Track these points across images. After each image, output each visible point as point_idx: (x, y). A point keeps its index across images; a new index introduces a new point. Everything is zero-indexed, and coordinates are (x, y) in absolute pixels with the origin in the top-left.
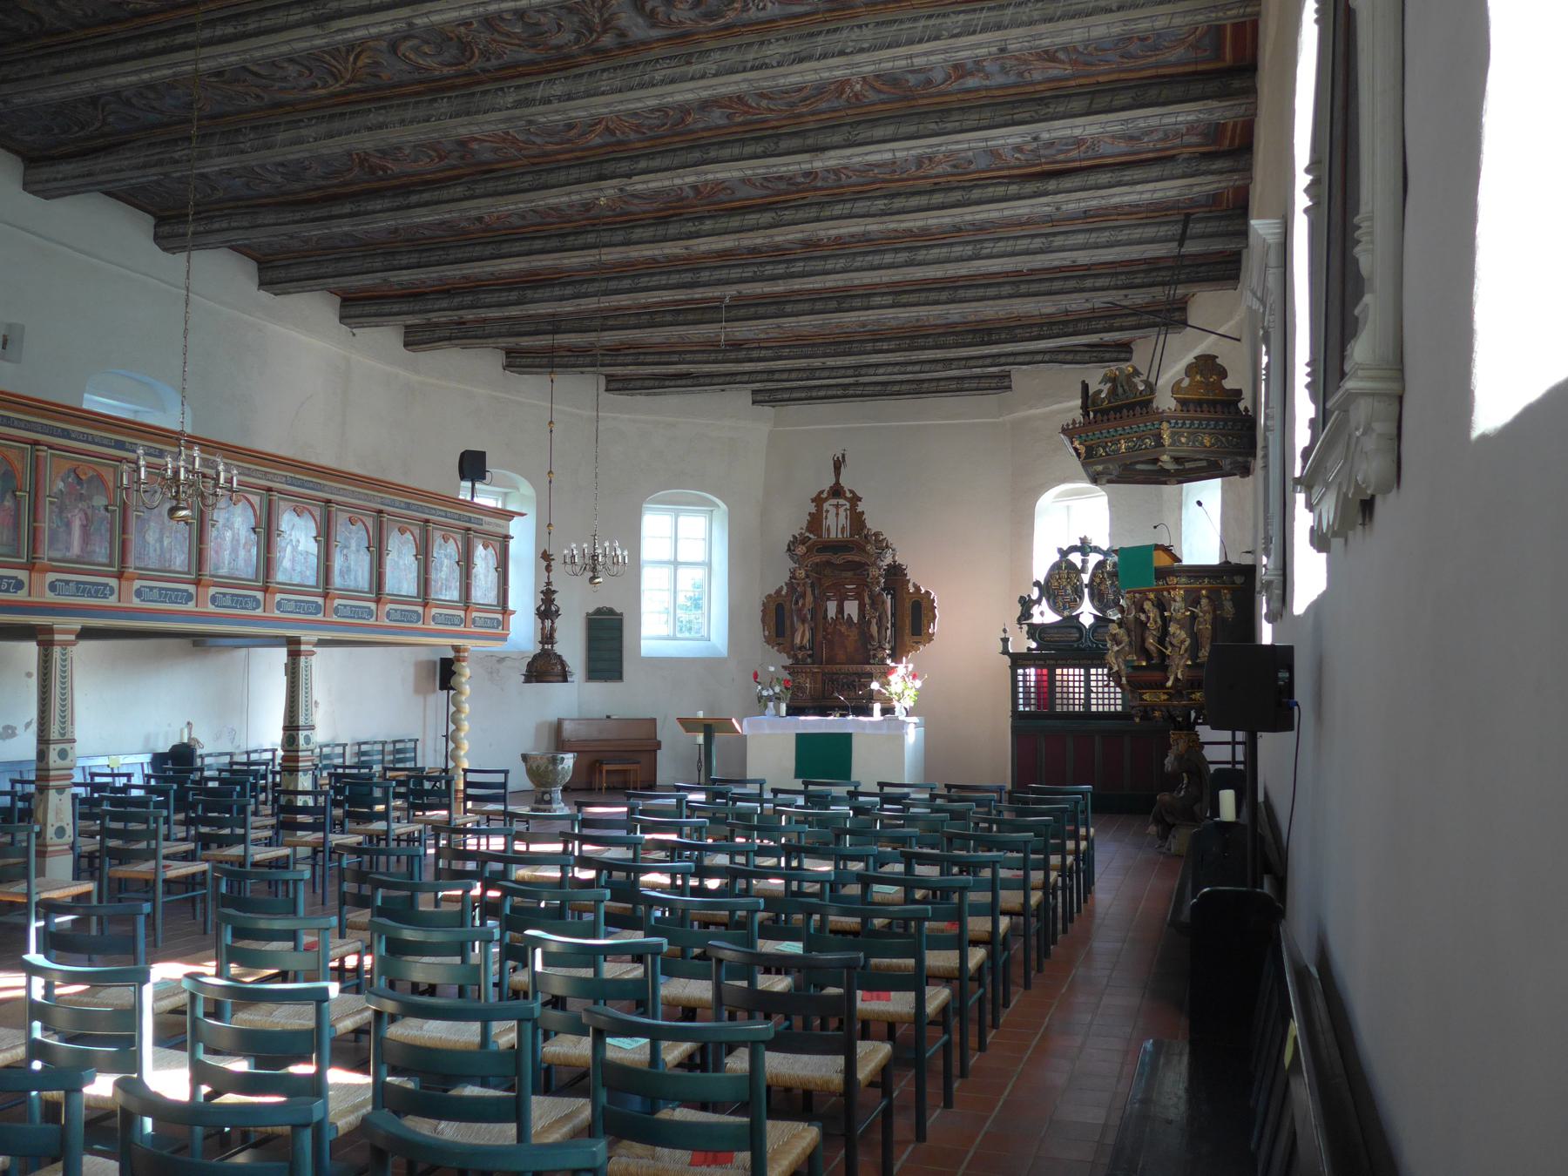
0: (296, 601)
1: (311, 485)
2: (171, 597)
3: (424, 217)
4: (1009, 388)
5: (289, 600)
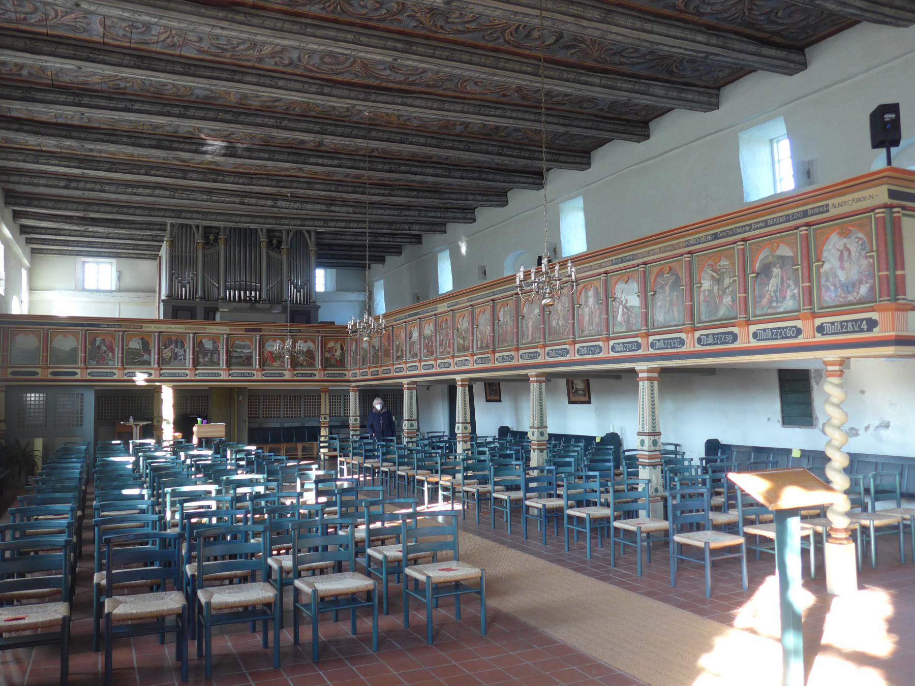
0: (623, 343)
1: (629, 258)
2: (721, 340)
3: (515, 80)
5: (619, 344)
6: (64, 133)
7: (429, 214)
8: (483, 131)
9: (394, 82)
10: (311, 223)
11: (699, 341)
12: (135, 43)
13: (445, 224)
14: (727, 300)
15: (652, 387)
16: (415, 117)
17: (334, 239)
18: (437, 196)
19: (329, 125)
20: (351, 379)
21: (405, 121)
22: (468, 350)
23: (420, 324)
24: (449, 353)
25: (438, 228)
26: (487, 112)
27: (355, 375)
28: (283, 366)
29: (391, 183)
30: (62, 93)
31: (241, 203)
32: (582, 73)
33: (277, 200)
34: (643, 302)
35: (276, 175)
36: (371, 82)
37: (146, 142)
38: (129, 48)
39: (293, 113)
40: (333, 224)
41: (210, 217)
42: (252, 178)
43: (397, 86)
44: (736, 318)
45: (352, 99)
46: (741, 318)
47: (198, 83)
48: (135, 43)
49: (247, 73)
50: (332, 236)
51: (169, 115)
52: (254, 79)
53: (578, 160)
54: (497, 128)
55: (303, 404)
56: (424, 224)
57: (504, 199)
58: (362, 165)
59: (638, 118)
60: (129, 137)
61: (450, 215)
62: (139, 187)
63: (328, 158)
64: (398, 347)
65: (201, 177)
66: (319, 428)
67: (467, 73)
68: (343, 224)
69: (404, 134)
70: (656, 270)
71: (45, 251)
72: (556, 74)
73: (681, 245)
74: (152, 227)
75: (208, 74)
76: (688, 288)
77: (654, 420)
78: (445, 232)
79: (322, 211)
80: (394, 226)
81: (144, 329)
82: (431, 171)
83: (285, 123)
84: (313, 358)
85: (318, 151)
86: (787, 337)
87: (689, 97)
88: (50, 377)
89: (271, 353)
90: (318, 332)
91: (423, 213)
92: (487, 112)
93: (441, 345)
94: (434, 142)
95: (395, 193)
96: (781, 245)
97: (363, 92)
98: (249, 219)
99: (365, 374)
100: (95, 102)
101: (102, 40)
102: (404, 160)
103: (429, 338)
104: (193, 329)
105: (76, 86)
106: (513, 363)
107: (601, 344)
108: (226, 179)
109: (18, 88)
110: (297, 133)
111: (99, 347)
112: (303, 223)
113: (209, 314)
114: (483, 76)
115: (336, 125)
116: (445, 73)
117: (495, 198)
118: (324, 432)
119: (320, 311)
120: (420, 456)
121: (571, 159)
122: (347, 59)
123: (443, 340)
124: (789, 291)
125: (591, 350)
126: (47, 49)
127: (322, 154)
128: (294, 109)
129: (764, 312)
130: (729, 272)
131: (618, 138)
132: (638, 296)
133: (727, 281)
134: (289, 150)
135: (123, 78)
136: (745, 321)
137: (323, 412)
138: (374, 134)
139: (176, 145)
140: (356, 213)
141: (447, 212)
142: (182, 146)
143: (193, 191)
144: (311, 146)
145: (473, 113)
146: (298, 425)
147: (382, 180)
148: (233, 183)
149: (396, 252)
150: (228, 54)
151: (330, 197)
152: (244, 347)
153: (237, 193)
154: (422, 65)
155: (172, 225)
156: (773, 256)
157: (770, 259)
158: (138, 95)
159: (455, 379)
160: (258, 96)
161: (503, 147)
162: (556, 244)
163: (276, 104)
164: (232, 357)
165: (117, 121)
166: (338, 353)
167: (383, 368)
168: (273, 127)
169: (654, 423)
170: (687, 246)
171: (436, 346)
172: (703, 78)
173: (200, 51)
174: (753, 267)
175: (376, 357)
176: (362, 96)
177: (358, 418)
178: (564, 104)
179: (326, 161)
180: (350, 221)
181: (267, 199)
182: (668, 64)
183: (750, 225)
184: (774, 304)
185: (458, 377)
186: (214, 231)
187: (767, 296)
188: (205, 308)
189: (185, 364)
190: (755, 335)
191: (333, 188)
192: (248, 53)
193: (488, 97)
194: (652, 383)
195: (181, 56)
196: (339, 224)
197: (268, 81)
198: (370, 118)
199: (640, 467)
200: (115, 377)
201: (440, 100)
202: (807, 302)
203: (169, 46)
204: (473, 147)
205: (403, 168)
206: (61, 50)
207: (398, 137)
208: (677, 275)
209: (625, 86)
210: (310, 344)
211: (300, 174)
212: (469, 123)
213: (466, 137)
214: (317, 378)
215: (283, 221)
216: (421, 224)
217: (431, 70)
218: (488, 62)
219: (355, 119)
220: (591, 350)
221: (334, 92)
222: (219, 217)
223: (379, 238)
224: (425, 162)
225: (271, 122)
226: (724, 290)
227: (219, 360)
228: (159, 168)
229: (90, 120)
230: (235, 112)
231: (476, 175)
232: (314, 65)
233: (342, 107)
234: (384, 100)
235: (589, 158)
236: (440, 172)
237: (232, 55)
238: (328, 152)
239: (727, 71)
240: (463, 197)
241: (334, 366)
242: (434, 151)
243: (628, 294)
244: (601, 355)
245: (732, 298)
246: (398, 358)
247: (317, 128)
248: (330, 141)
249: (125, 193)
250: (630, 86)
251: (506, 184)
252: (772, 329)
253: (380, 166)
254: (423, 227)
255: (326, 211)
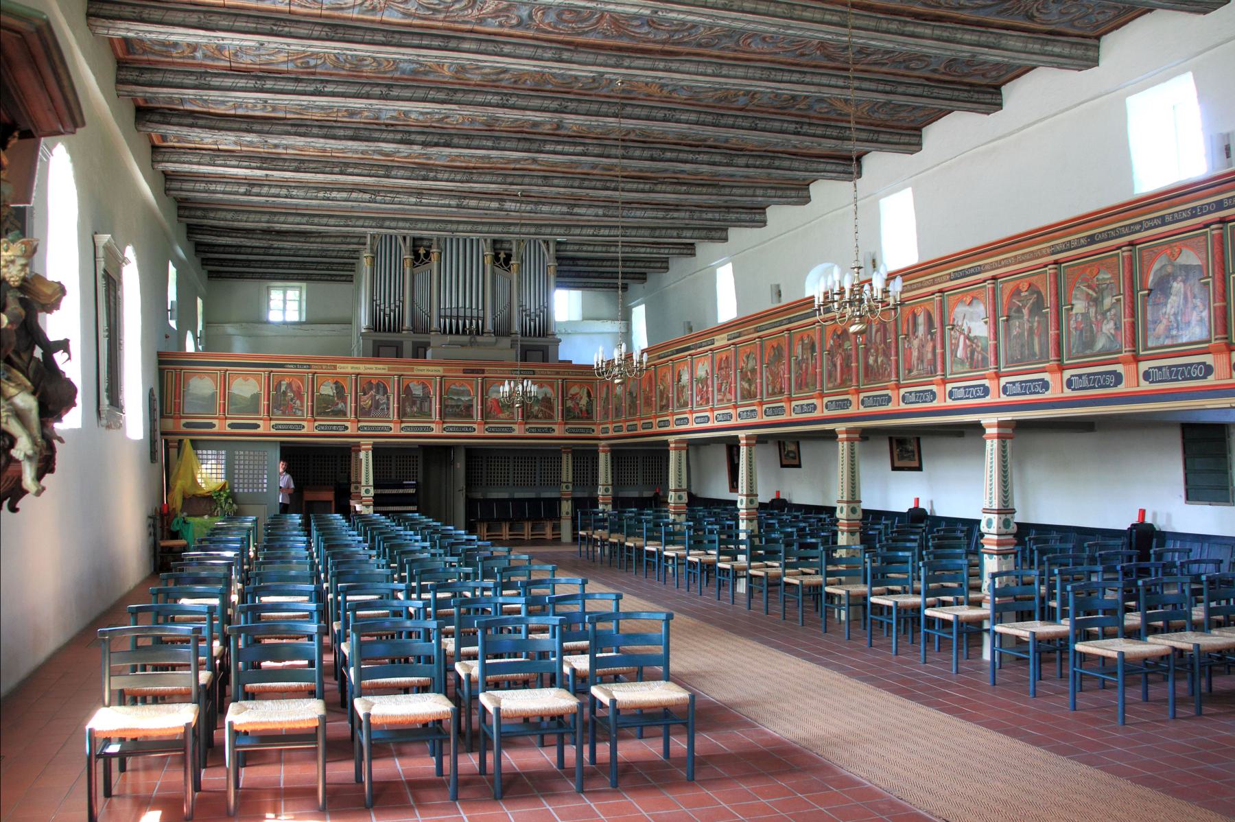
0: (965, 387)
1: (972, 270)
2: (1099, 381)
4: (694, 255)
5: (959, 388)
6: (244, 126)
7: (704, 216)
8: (775, 103)
9: (655, 42)
10: (548, 230)
11: (1069, 383)
12: (327, 9)
13: (726, 230)
14: (1108, 327)
15: (1004, 447)
16: (682, 87)
17: (578, 251)
18: (714, 191)
19: (571, 100)
20: (601, 435)
21: (670, 92)
22: (755, 396)
23: (692, 362)
24: (729, 401)
25: (718, 234)
26: (779, 76)
27: (606, 430)
28: (512, 418)
29: (653, 175)
30: (242, 77)
31: (458, 206)
32: (908, 22)
33: (504, 201)
34: (992, 330)
35: (502, 169)
36: (624, 42)
37: (341, 132)
38: (320, 16)
39: (524, 86)
40: (578, 231)
41: (419, 225)
42: (472, 173)
43: (658, 47)
44: (1121, 352)
45: (600, 65)
46: (1126, 353)
47: (404, 54)
48: (327, 9)
49: (464, 39)
50: (576, 247)
51: (368, 97)
52: (473, 46)
53: (905, 139)
54: (793, 98)
55: (538, 468)
56: (699, 229)
57: (805, 193)
58: (613, 151)
59: (984, 82)
60: (320, 127)
61: (733, 216)
62: (332, 190)
63: (570, 143)
64: (662, 393)
65: (408, 174)
66: (559, 500)
67: (751, 26)
68: (590, 231)
69: (670, 109)
70: (1011, 286)
71: (223, 275)
72: (872, 24)
73: (1044, 252)
74: (348, 240)
75: (416, 42)
76: (1054, 311)
77: (1005, 492)
78: (726, 239)
79: (562, 214)
80: (657, 233)
81: (338, 370)
82: (705, 158)
83: (513, 100)
84: (551, 409)
85: (558, 136)
86: (1191, 378)
87: (1057, 50)
88: (229, 430)
89: (497, 401)
90: (558, 373)
91: (697, 215)
92: (779, 78)
93: (719, 390)
94: (709, 119)
95: (659, 187)
96: (1185, 250)
97: (615, 56)
98: (469, 227)
99: (619, 429)
100: (281, 85)
101: (287, 8)
102: (669, 143)
103: (704, 381)
104: (398, 369)
105: (258, 67)
106: (816, 414)
107: (934, 388)
108: (440, 176)
109: (192, 73)
110: (528, 113)
111: (285, 393)
112: (538, 230)
113: (419, 351)
114: (773, 29)
115: (579, 101)
116: (722, 26)
117: (793, 193)
118: (566, 507)
119: (561, 346)
120: (649, 525)
121: (895, 139)
122: (592, 14)
123: (722, 384)
124: (1195, 313)
125: (921, 396)
126: (224, 23)
127: (561, 139)
128: (525, 82)
129: (1159, 343)
130: (1112, 289)
131: (959, 109)
132: (986, 323)
133: (1108, 301)
134: (519, 136)
135: (313, 54)
136: (1226, 344)
137: (564, 479)
138: (629, 110)
139: (376, 135)
140: (607, 216)
141: (728, 213)
142: (384, 135)
143: (398, 193)
144: (547, 128)
145: (761, 79)
146: (532, 495)
147: (641, 171)
148: (447, 181)
149: (660, 268)
150: (441, 16)
151: (572, 194)
152: (462, 393)
153: (454, 193)
154: (690, 18)
155: (373, 237)
156: (1173, 266)
157: (1169, 269)
158: (331, 75)
159: (737, 437)
160: (478, 68)
161: (802, 123)
162: (874, 254)
163: (502, 76)
164: (446, 406)
165: (307, 108)
166: (584, 402)
167: (658, 420)
168: (497, 106)
169: (1006, 497)
170: (1053, 253)
171: (713, 391)
172: (1076, 23)
173: (406, 14)
174: (1143, 281)
175: (633, 405)
176: (612, 61)
177: (610, 487)
178: (884, 64)
179: (567, 148)
180: (600, 227)
181: (491, 200)
182: (1026, 6)
183: (1140, 223)
184: (1174, 332)
185: (741, 434)
186: (425, 243)
187: (1165, 321)
188: (414, 343)
189: (388, 414)
190: (1147, 376)
191: (576, 183)
192: (466, 13)
193: (781, 58)
194: (1004, 442)
195: (382, 22)
196: (584, 231)
197: (491, 47)
198: (623, 90)
199: (985, 556)
200: (304, 431)
201: (716, 63)
202: (1220, 329)
203: (368, 11)
204: (761, 124)
205: (668, 155)
206: (240, 24)
207: (661, 114)
208: (1039, 293)
209: (967, 37)
210: (547, 390)
211: (533, 167)
212: (756, 93)
213: (752, 111)
214: (556, 434)
215: (512, 229)
216: (694, 229)
217: (703, 23)
218: (779, 10)
219: (604, 92)
220: (921, 396)
221: (576, 57)
222: (431, 226)
223: (637, 250)
224: (697, 146)
225: (495, 99)
226: (1104, 314)
227: (430, 410)
228: (356, 165)
229: (274, 109)
230: (450, 89)
231: (766, 162)
232: (549, 24)
233: (586, 77)
234: (641, 66)
235: (920, 136)
236: (717, 158)
237: (445, 17)
238: (570, 136)
239: (1111, 13)
240: (750, 192)
241: (579, 418)
242: (709, 131)
243: (971, 319)
244: (935, 404)
245: (1115, 324)
246: (662, 408)
247: (554, 105)
248: (573, 122)
249: (316, 198)
250: (974, 38)
251: (807, 174)
252: (1170, 367)
253: (638, 153)
254: (696, 233)
255: (568, 214)
